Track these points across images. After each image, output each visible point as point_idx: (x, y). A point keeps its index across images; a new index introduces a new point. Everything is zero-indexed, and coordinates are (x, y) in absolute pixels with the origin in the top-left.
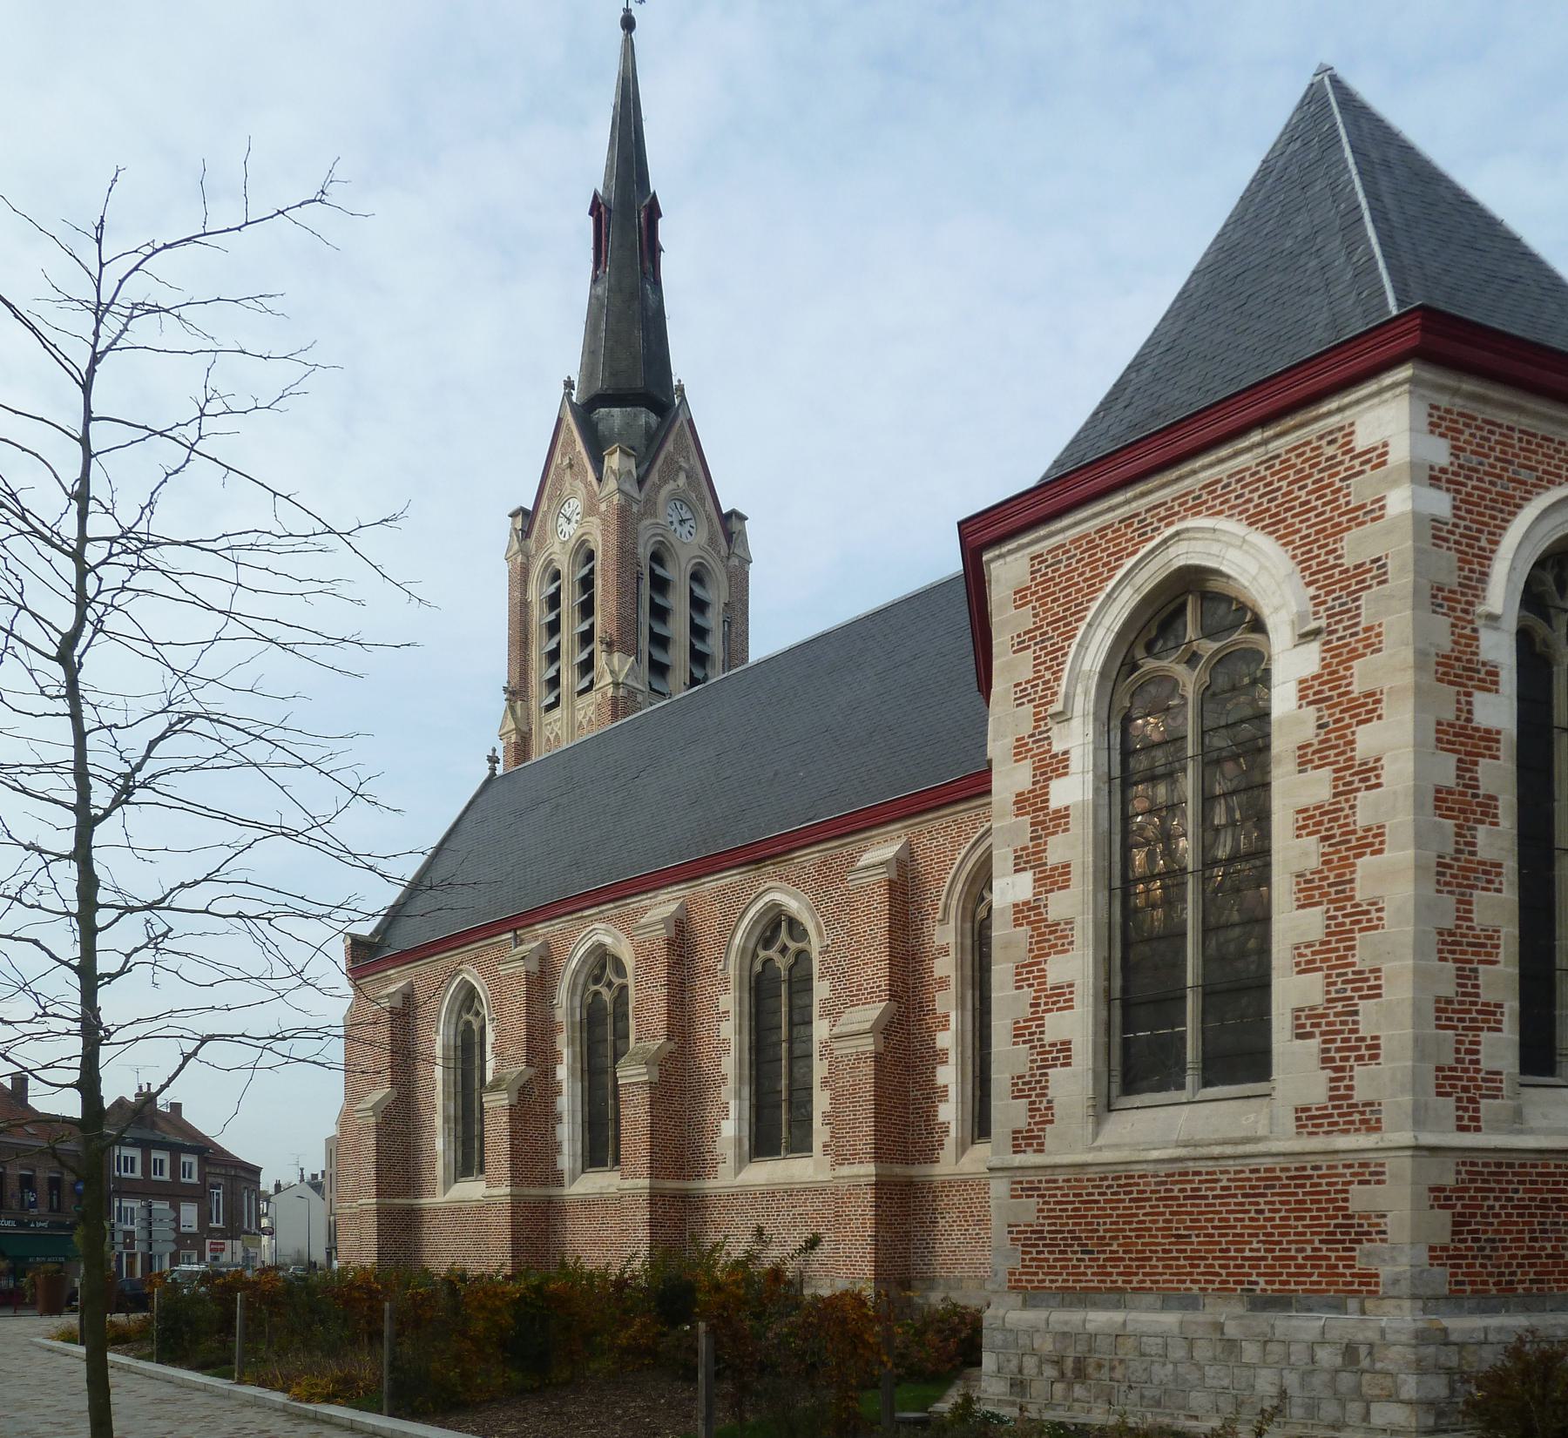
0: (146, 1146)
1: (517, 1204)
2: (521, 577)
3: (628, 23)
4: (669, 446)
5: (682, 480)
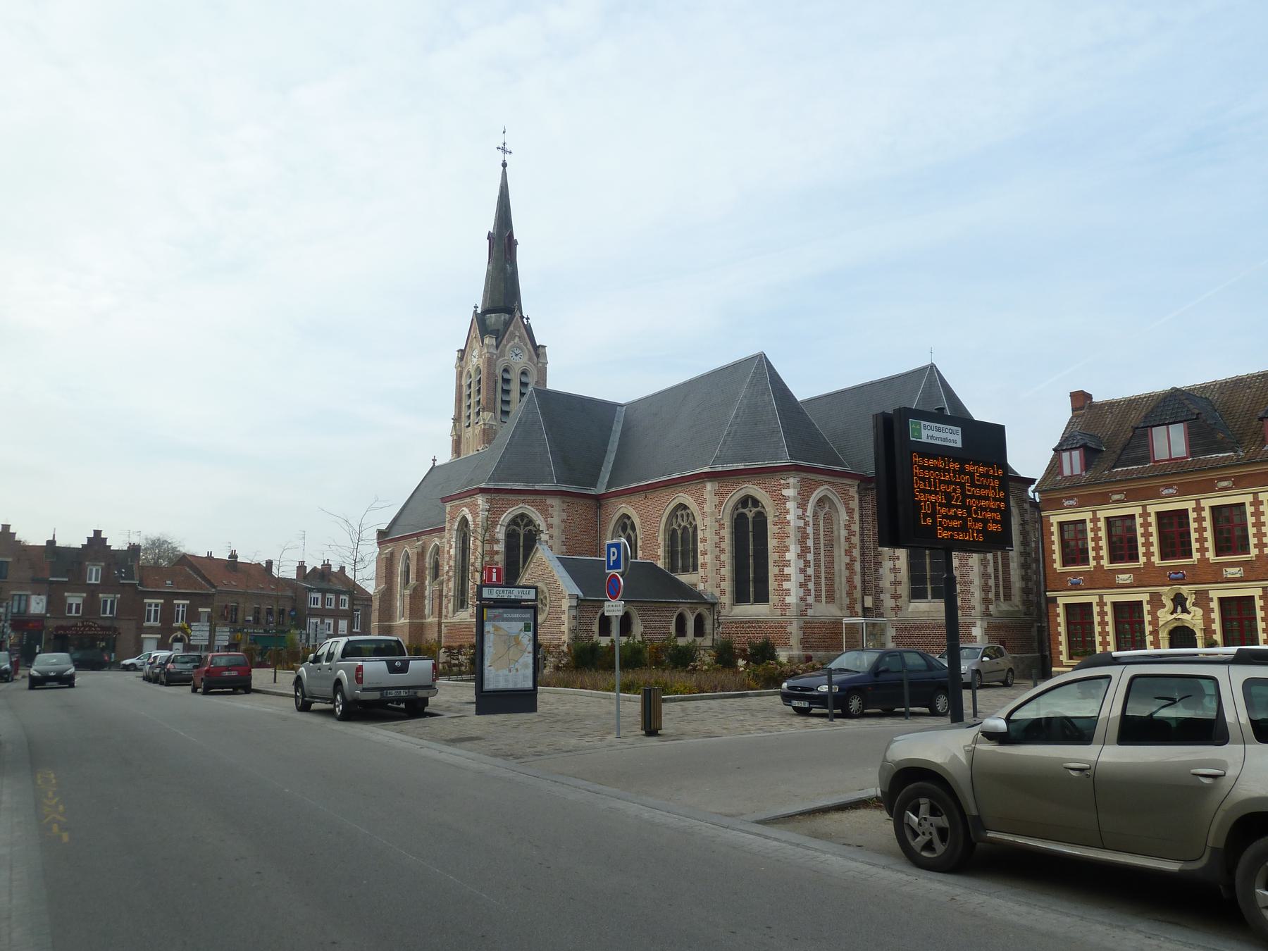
0: (324, 592)
1: (411, 625)
2: (460, 376)
3: (504, 165)
4: (511, 328)
5: (517, 340)
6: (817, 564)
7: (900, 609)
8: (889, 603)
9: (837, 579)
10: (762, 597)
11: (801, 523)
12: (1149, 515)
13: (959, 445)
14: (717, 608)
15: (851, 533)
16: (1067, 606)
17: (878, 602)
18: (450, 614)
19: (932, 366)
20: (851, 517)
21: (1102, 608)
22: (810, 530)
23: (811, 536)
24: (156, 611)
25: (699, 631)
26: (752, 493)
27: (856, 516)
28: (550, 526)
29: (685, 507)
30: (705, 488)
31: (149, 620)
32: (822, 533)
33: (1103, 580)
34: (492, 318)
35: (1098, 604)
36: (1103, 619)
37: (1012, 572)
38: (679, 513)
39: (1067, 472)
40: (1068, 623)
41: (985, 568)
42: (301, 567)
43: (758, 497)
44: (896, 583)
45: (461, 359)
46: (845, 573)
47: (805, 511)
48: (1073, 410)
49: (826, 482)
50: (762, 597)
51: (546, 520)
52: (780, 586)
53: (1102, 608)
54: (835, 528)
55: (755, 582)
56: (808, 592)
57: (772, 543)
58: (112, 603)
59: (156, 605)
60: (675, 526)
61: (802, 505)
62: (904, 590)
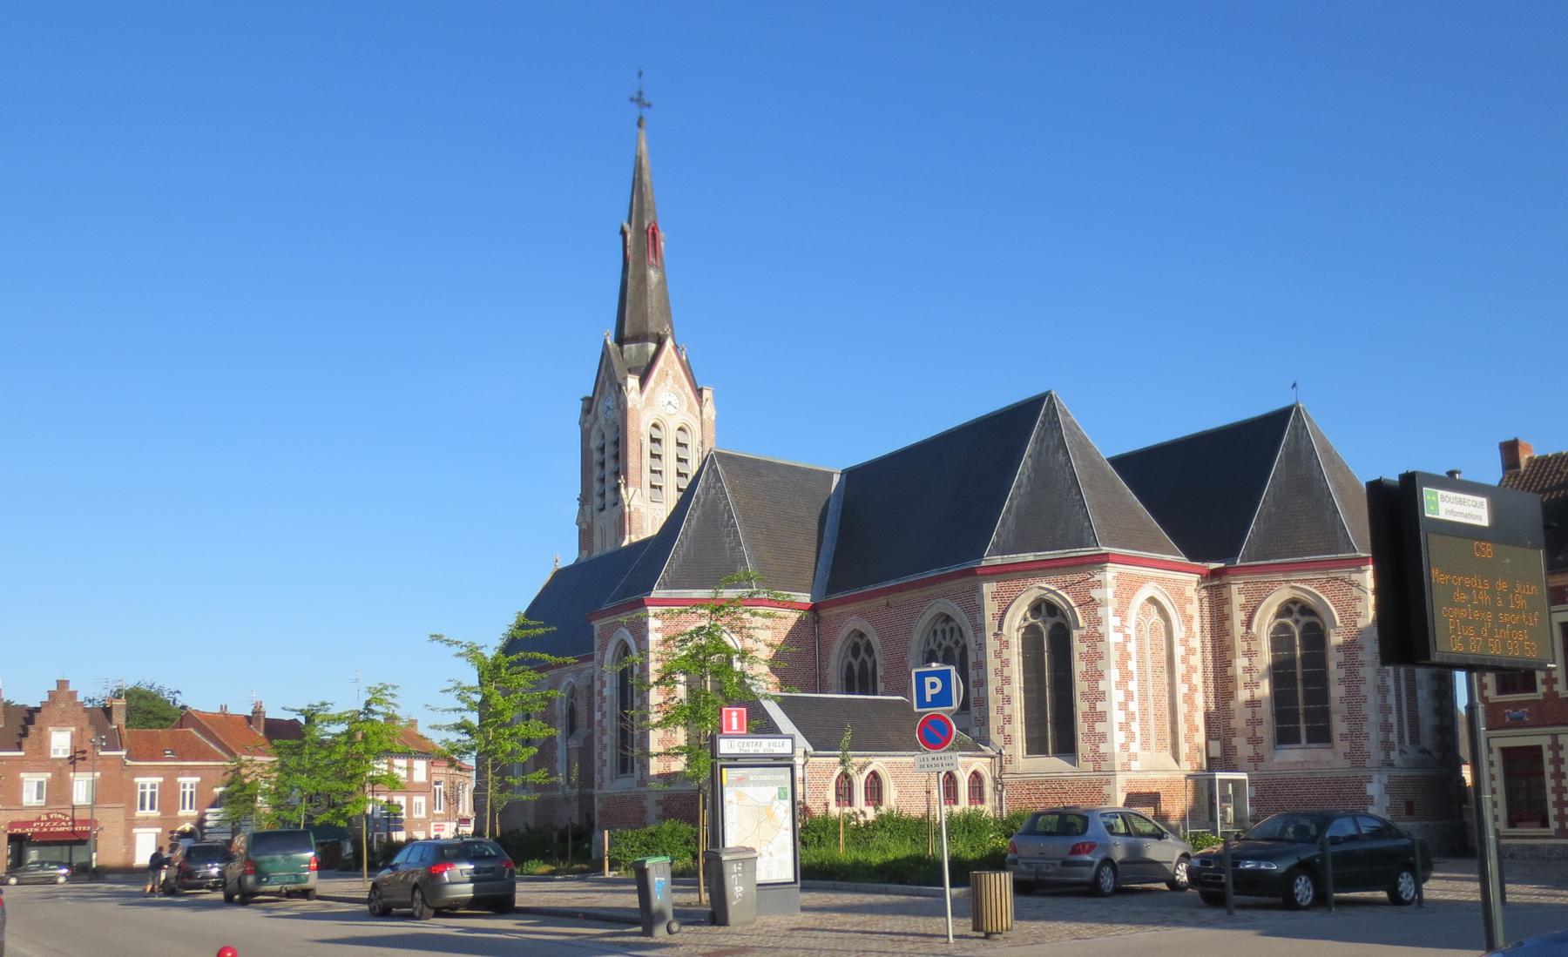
2: (585, 436)
6: (1144, 697)
13: (1484, 521)
20: (1189, 629)
23: (1134, 656)
24: (152, 794)
31: (143, 807)
37: (1421, 703)
59: (153, 786)
62: (1266, 731)
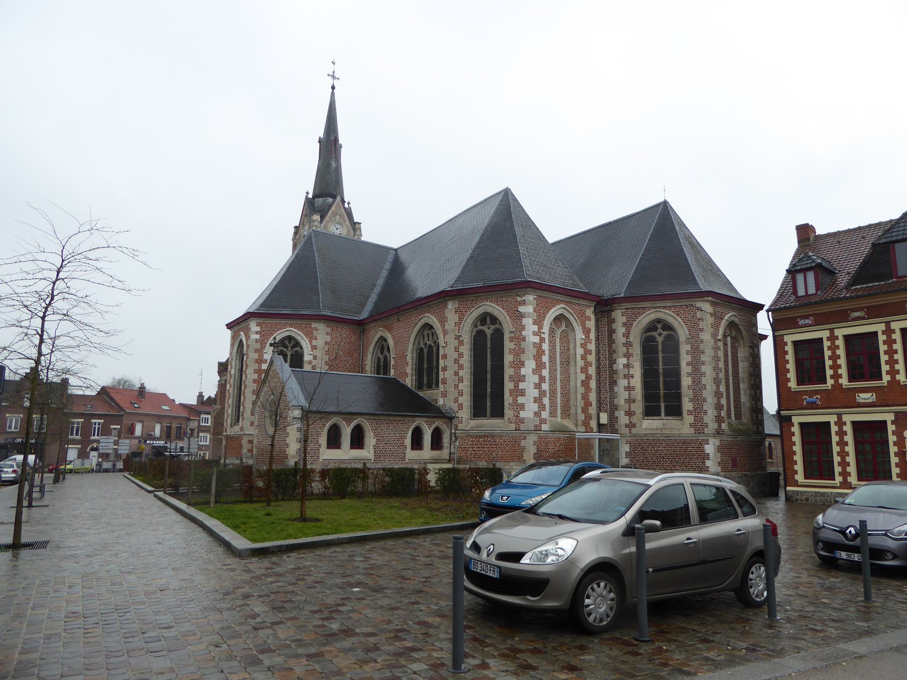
3: (333, 88)
7: (634, 426)
8: (623, 419)
9: (572, 396)
10: (498, 412)
11: (537, 339)
12: (894, 332)
14: (455, 422)
15: (587, 352)
16: (802, 425)
17: (613, 419)
18: (228, 430)
19: (665, 203)
20: (588, 337)
21: (841, 428)
22: (546, 347)
23: (547, 353)
25: (437, 443)
26: (490, 310)
27: (593, 336)
28: (314, 348)
29: (431, 327)
30: (446, 307)
32: (558, 351)
33: (842, 399)
34: (319, 201)
35: (836, 424)
36: (841, 439)
38: (425, 333)
39: (801, 292)
40: (857, 442)
41: (718, 386)
42: (201, 396)
43: (496, 313)
44: (630, 401)
45: (296, 233)
46: (581, 390)
47: (540, 328)
48: (799, 242)
49: (562, 302)
50: (498, 412)
51: (311, 342)
52: (515, 400)
53: (841, 428)
54: (571, 346)
55: (492, 397)
56: (542, 407)
57: (508, 358)
58: (16, 421)
59: (78, 423)
60: (422, 345)
61: (539, 322)
62: (638, 407)
